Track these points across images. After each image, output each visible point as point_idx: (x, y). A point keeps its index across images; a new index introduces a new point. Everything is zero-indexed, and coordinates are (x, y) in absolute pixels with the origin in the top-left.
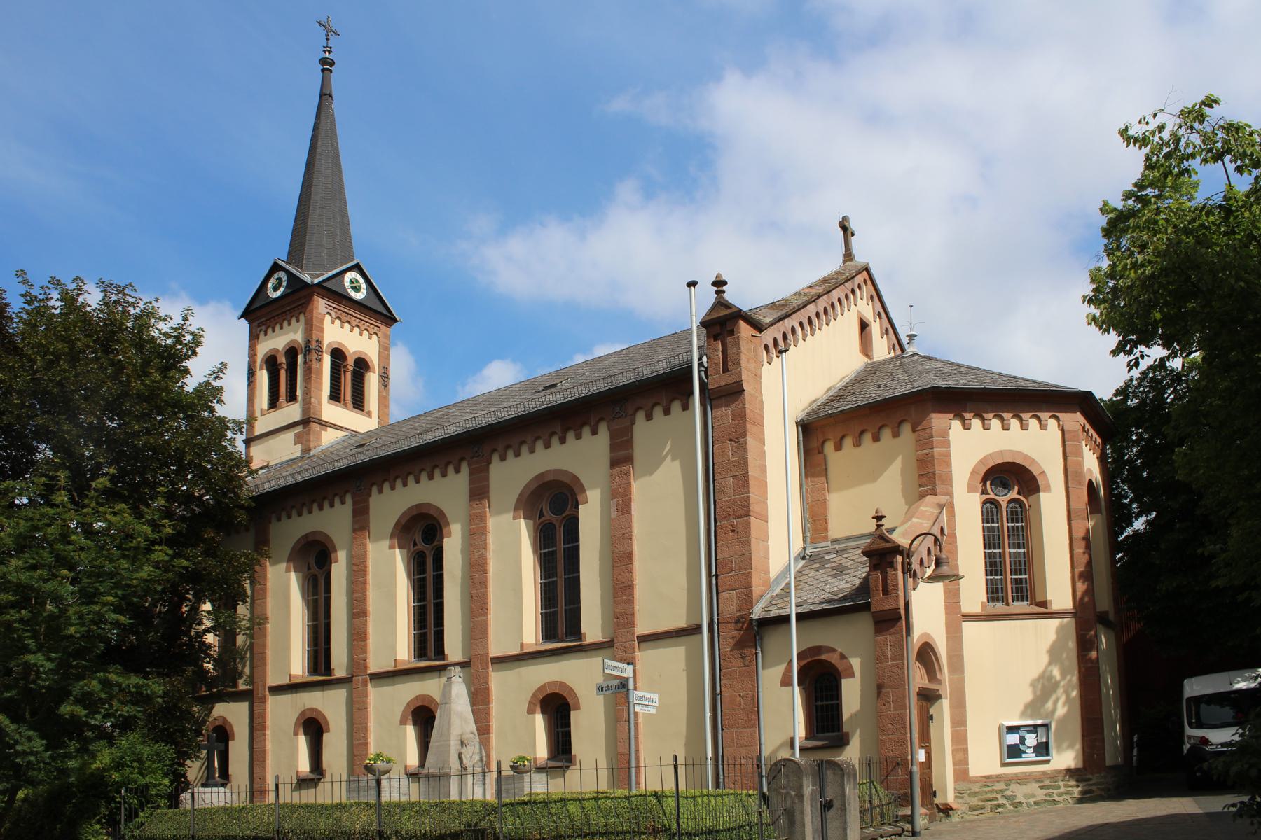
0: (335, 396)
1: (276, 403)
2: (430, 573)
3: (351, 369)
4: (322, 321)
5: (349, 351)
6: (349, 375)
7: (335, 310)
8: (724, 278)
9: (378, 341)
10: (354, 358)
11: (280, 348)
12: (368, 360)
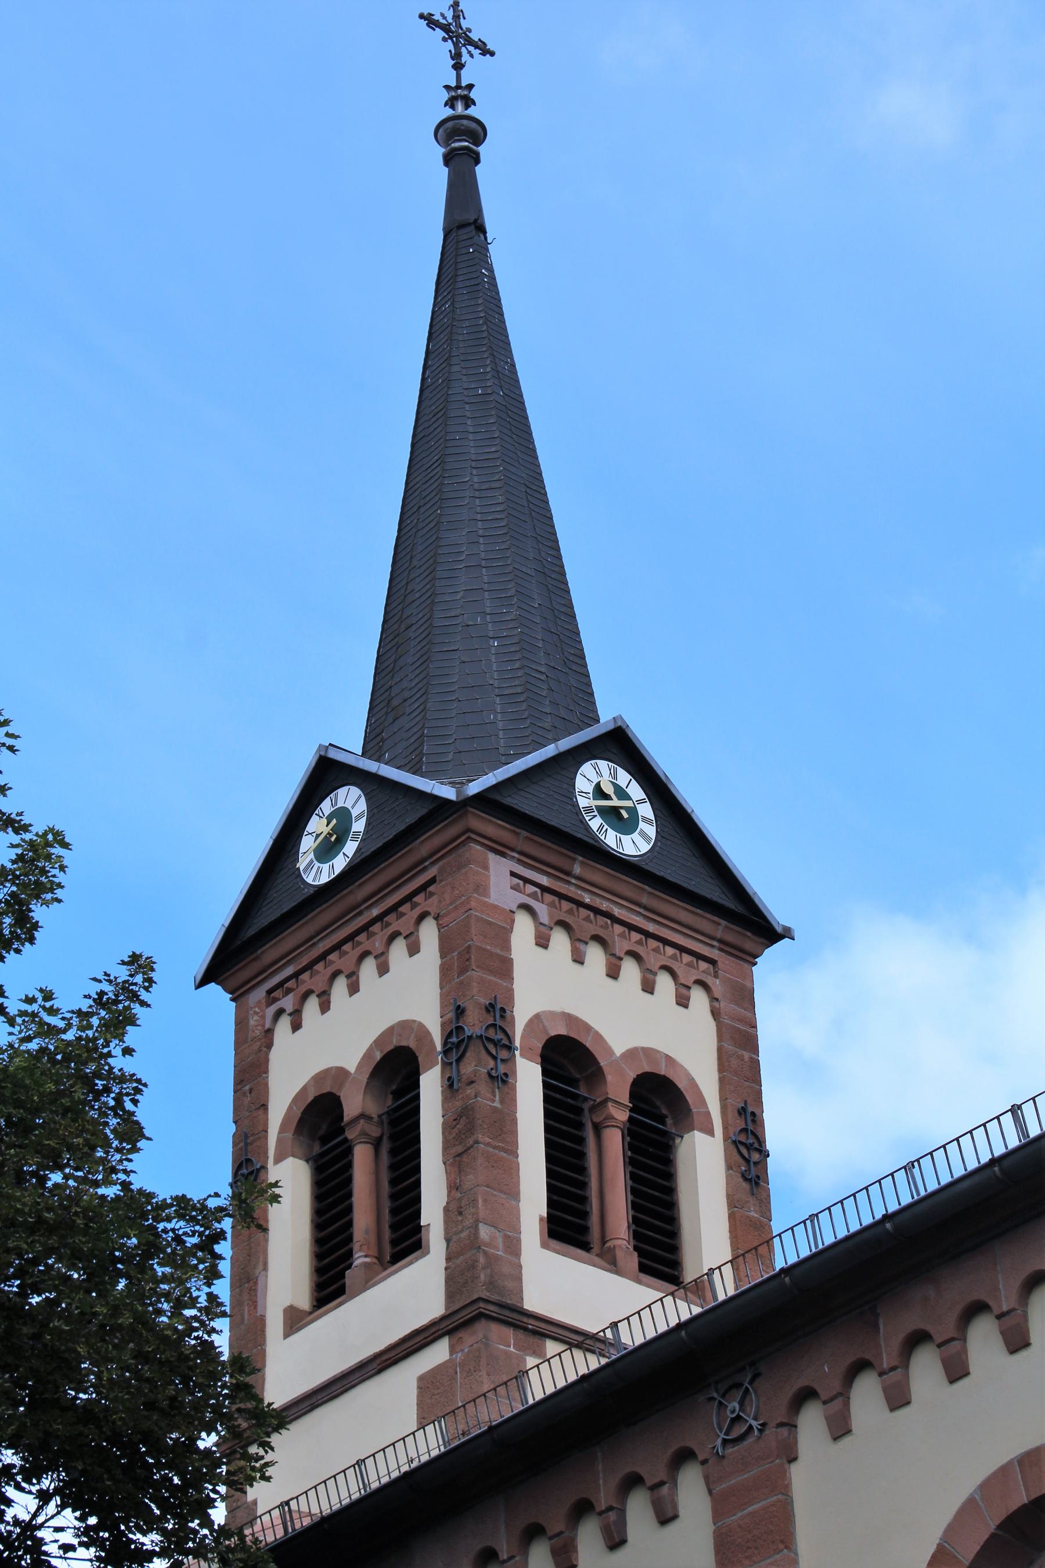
1: (342, 1275)
3: (622, 1116)
4: (503, 935)
5: (610, 1051)
6: (615, 1142)
7: (549, 898)
9: (715, 1013)
10: (632, 1075)
11: (351, 1066)
12: (682, 1084)
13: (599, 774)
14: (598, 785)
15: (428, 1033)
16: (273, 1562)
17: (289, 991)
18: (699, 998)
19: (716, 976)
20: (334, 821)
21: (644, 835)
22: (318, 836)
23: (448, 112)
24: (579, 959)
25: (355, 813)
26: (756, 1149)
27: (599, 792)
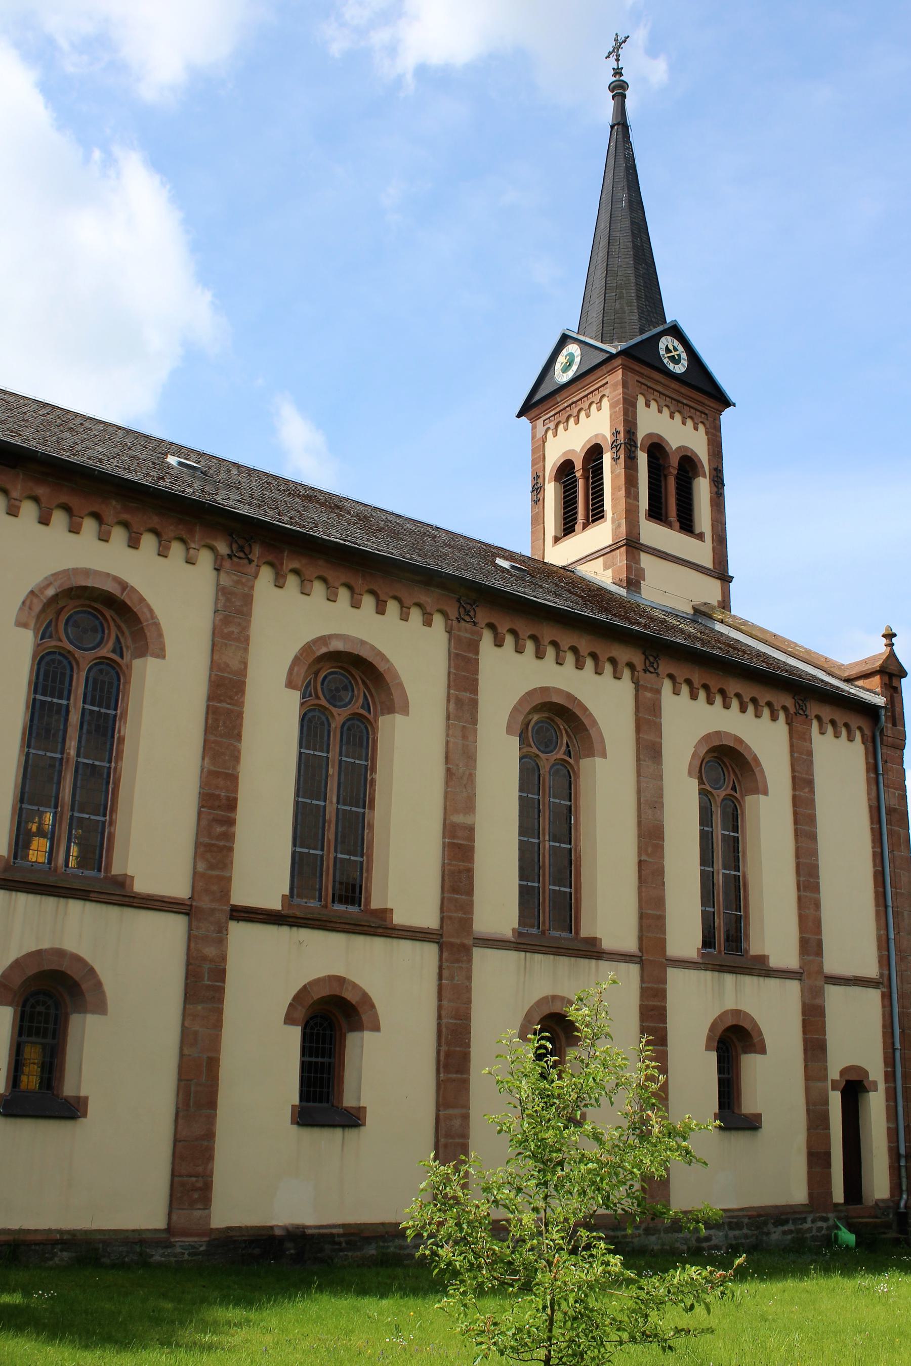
1: (574, 526)
2: (720, 873)
3: (675, 472)
8: (894, 631)
9: (707, 433)
11: (578, 450)
13: (668, 342)
15: (607, 438)
16: (692, 1267)
17: (552, 421)
19: (707, 420)
20: (568, 357)
22: (562, 363)
23: (614, 79)
24: (684, 423)
25: (576, 355)
26: (634, 446)
27: (668, 350)
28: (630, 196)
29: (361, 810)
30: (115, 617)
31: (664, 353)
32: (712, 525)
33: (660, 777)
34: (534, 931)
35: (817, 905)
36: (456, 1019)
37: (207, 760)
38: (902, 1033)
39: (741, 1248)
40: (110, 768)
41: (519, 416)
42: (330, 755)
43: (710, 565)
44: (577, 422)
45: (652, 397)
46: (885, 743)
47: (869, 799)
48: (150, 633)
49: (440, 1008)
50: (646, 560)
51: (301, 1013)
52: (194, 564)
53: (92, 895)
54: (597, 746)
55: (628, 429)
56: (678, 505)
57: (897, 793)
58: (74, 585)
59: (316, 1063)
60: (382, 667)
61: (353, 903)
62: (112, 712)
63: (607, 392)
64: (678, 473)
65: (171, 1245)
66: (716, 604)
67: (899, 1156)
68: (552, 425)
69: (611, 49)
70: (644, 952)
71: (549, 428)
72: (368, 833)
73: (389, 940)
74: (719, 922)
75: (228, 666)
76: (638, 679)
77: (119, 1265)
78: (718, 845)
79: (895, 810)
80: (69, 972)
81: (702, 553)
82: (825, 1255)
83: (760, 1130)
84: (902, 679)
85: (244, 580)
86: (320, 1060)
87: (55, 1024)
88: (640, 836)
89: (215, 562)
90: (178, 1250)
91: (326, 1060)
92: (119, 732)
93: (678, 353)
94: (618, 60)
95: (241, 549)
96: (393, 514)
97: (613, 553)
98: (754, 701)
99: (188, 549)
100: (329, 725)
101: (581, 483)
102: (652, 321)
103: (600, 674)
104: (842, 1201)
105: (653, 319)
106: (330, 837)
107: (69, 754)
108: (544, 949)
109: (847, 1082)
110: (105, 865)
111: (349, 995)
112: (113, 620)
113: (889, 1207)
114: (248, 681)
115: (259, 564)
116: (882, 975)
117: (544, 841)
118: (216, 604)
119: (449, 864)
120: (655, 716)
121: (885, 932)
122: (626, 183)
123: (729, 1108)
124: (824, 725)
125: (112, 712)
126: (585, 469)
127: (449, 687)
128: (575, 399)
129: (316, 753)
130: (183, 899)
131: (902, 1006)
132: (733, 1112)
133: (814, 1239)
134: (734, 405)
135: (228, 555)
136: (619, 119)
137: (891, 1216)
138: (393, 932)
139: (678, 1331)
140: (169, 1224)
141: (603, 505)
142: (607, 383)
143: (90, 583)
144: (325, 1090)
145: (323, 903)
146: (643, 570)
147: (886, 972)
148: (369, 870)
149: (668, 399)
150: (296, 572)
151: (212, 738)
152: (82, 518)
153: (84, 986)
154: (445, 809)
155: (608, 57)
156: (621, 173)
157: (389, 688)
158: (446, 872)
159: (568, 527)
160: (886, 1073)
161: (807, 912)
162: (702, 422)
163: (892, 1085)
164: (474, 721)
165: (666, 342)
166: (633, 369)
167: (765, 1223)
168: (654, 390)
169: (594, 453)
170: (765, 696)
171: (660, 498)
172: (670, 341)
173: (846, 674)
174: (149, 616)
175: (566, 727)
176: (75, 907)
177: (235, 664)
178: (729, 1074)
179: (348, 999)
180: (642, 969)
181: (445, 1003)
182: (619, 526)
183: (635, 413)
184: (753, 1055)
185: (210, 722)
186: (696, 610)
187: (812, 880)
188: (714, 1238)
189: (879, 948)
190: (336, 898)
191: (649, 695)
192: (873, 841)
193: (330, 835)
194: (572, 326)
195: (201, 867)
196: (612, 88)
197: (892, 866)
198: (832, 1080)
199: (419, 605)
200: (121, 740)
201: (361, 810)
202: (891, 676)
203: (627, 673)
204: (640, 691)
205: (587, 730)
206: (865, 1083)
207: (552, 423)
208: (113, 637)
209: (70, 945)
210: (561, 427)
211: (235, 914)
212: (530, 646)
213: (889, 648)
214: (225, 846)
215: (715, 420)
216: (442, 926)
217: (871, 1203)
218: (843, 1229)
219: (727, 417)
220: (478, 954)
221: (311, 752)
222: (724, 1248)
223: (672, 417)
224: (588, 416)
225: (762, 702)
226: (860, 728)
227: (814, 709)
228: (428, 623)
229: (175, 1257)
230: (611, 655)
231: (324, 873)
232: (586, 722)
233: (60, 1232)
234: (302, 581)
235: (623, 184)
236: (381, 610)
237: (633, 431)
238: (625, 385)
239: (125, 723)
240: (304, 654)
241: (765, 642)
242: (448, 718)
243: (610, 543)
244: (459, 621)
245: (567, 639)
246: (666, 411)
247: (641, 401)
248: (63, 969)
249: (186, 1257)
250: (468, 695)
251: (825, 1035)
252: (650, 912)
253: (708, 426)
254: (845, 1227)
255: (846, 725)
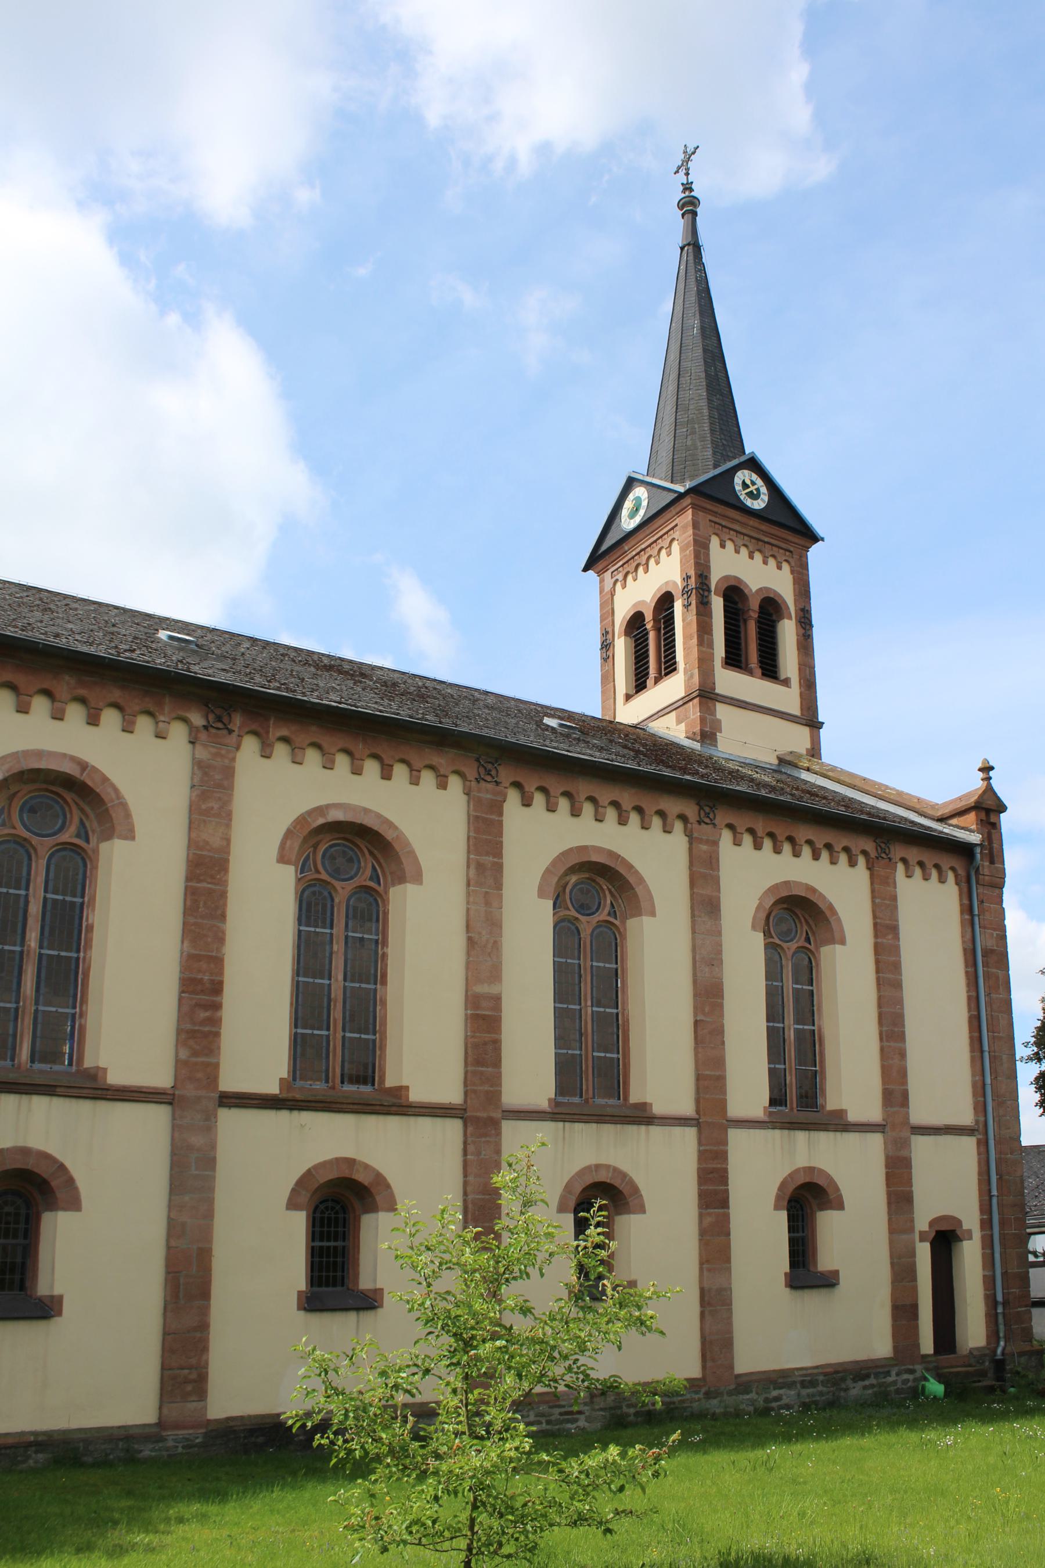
0: (734, 659)
1: (645, 681)
2: (791, 1028)
3: (755, 615)
8: (991, 764)
9: (792, 572)
11: (648, 601)
13: (744, 476)
14: (744, 481)
18: (786, 566)
21: (763, 500)
23: (683, 195)
24: (765, 563)
27: (745, 485)
28: (702, 322)
29: (372, 986)
30: (78, 800)
31: (741, 488)
32: (800, 669)
33: (719, 933)
34: (576, 1100)
35: (903, 1055)
36: (484, 1194)
37: (186, 944)
38: (1000, 1179)
39: (813, 1406)
40: (78, 959)
41: (585, 569)
42: (334, 931)
43: (797, 712)
44: (646, 571)
45: (728, 536)
46: (981, 882)
47: (963, 942)
48: (117, 815)
49: (465, 1184)
50: (722, 711)
51: (304, 1197)
52: (164, 738)
53: (58, 1090)
54: (644, 904)
55: (700, 572)
56: (759, 650)
57: (995, 933)
58: (25, 768)
59: (328, 1248)
60: (389, 835)
61: (365, 1083)
62: (78, 900)
63: (676, 534)
64: (759, 617)
65: (162, 1439)
66: (804, 752)
67: (995, 1303)
68: (620, 577)
69: (680, 163)
70: (701, 1113)
71: (617, 580)
72: (380, 1010)
73: (404, 1119)
74: (791, 1079)
75: (207, 843)
76: (691, 831)
77: (103, 1463)
78: (788, 1000)
79: (992, 951)
80: (36, 1170)
81: (789, 699)
82: (909, 1407)
83: (837, 1286)
84: (1001, 815)
85: (223, 752)
86: (332, 1244)
87: (27, 1222)
88: (696, 995)
89: (190, 734)
90: (170, 1443)
91: (340, 1244)
92: (87, 920)
93: (756, 487)
94: (687, 174)
95: (219, 719)
96: (435, 680)
97: (686, 706)
98: (828, 846)
99: (157, 723)
100: (332, 900)
101: (652, 636)
102: (728, 456)
103: (647, 829)
104: (931, 1351)
105: (729, 454)
106: (336, 1016)
107: (29, 946)
108: (585, 1117)
109: (938, 1232)
110: (77, 1059)
111: (360, 1177)
112: (77, 804)
113: (985, 1355)
114: (231, 859)
115: (241, 734)
116: (977, 1122)
117: (586, 1006)
118: (192, 779)
119: (472, 1037)
120: (712, 869)
121: (981, 1078)
122: (697, 309)
123: (804, 1266)
124: (911, 867)
125: (78, 900)
126: (655, 620)
127: (469, 852)
128: (643, 546)
129: (318, 930)
130: (165, 1089)
131: (999, 1152)
132: (809, 1271)
133: (898, 1391)
134: (823, 539)
135: (204, 726)
136: (690, 239)
137: (987, 1364)
138: (410, 1109)
139: (617, 1513)
140: (160, 1418)
141: (674, 657)
142: (676, 525)
143: (43, 765)
144: (339, 1274)
145: (330, 1084)
146: (719, 721)
147: (982, 1119)
148: (383, 1048)
149: (746, 538)
150: (285, 740)
151: (192, 920)
152: (30, 696)
153: (53, 1184)
154: (467, 979)
155: (677, 172)
156: (692, 297)
157: (399, 857)
158: (469, 1045)
159: (640, 684)
160: (982, 1222)
161: (891, 1062)
162: (786, 561)
163: (988, 1232)
164: (499, 885)
165: (742, 476)
166: (706, 509)
167: (843, 1380)
168: (730, 529)
169: (665, 601)
170: (841, 840)
171: (739, 644)
172: (747, 475)
173: (939, 814)
174: (114, 796)
175: (610, 887)
176: (40, 1104)
177: (216, 842)
178: (803, 1232)
179: (360, 1180)
180: (465, 1126)
181: (471, 1178)
182: (692, 676)
183: (707, 555)
184: (829, 1212)
185: (188, 903)
186: (781, 761)
187: (896, 1029)
188: (784, 1397)
189: (975, 1095)
190: (346, 1079)
191: (704, 847)
192: (968, 985)
193: (337, 1013)
194: (640, 467)
195: (184, 1054)
196: (681, 206)
197: (989, 1009)
198: (920, 1232)
199: (431, 767)
200: (90, 928)
201: (372, 986)
202: (988, 811)
203: (678, 826)
204: (694, 845)
205: (633, 889)
206: (959, 1233)
207: (620, 574)
208: (76, 821)
209: (36, 1143)
210: (630, 578)
211: (225, 1100)
212: (564, 804)
213: (986, 782)
214: (210, 1032)
215: (801, 557)
216: (465, 1101)
217: (965, 1352)
218: (932, 1380)
219: (815, 554)
220: (508, 1127)
221: (312, 929)
222: (796, 1407)
223: (751, 557)
224: (657, 563)
225: (838, 847)
226: (953, 869)
227: (898, 851)
228: (443, 785)
229: (167, 1451)
230: (660, 807)
231: (331, 1054)
232: (632, 880)
233: (35, 1433)
234: (293, 750)
235: (693, 309)
236: (386, 774)
237: (705, 574)
238: (695, 525)
239: (93, 910)
240: (298, 827)
241: (853, 787)
242: (468, 884)
243: (683, 695)
244: (478, 782)
245: (606, 793)
246: (744, 551)
247: (715, 542)
248: (29, 1167)
249: (180, 1450)
250: (491, 858)
251: (912, 1186)
252: (707, 1073)
253: (793, 564)
254: (935, 1379)
255: (937, 866)
